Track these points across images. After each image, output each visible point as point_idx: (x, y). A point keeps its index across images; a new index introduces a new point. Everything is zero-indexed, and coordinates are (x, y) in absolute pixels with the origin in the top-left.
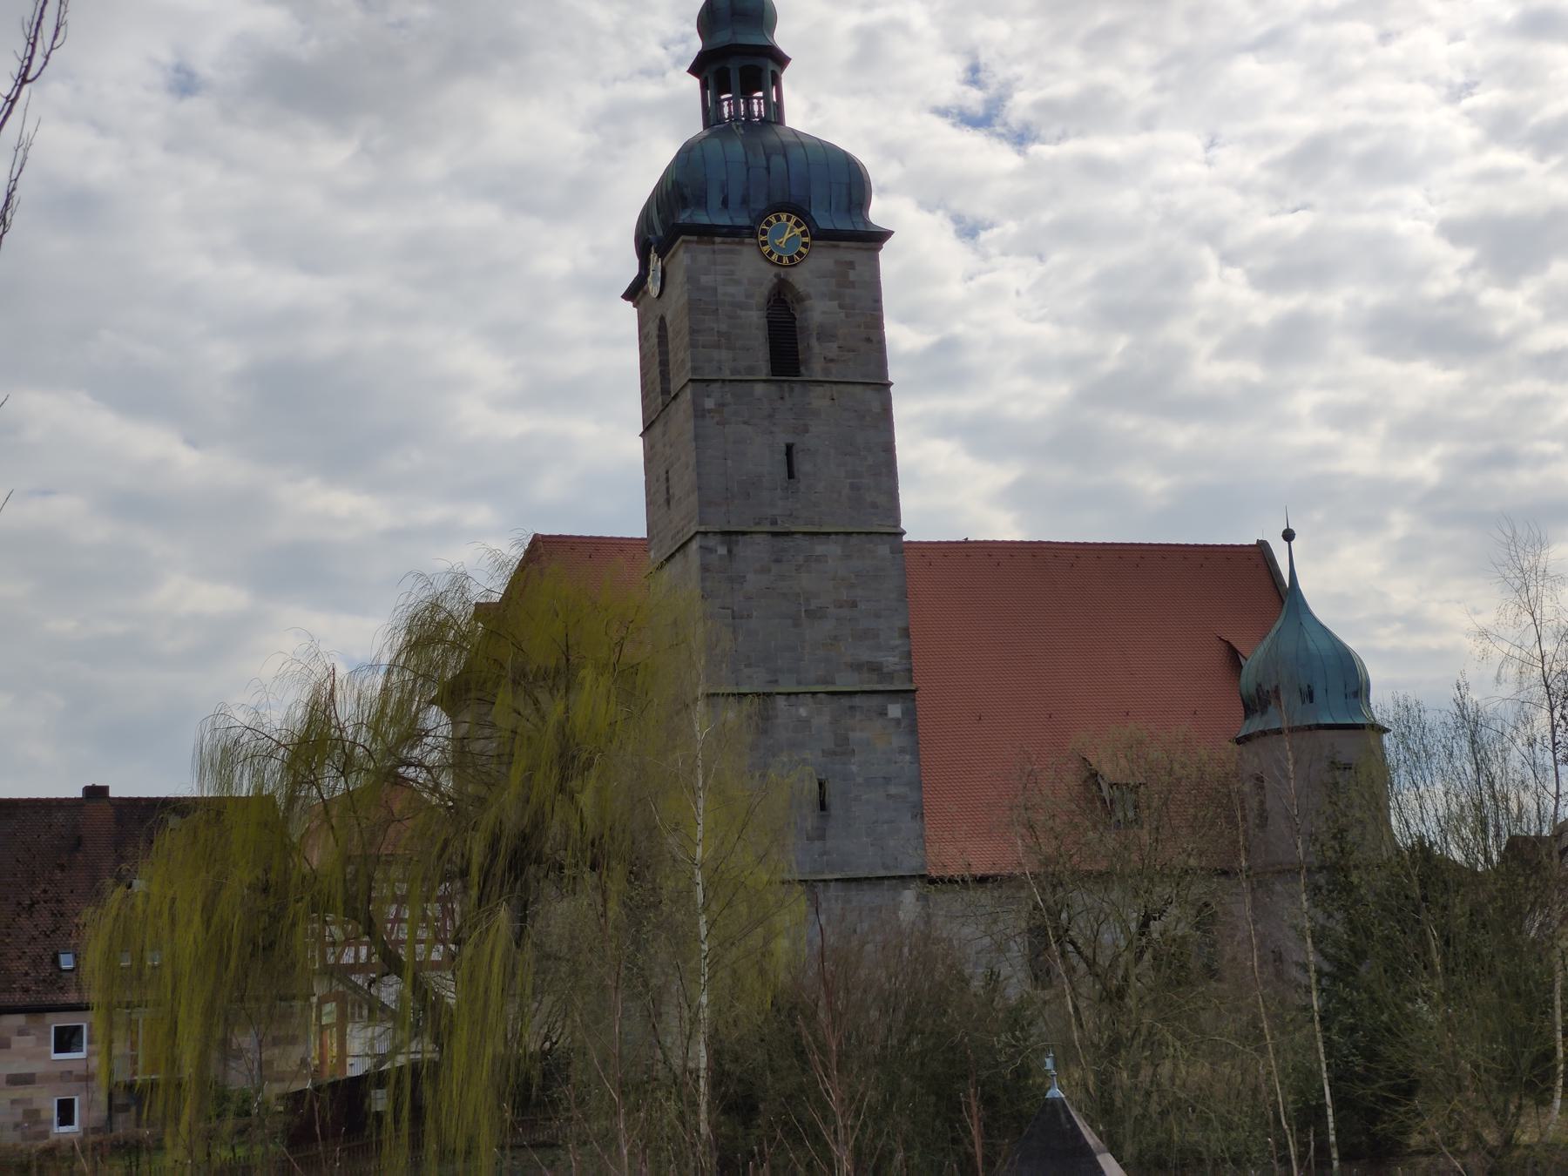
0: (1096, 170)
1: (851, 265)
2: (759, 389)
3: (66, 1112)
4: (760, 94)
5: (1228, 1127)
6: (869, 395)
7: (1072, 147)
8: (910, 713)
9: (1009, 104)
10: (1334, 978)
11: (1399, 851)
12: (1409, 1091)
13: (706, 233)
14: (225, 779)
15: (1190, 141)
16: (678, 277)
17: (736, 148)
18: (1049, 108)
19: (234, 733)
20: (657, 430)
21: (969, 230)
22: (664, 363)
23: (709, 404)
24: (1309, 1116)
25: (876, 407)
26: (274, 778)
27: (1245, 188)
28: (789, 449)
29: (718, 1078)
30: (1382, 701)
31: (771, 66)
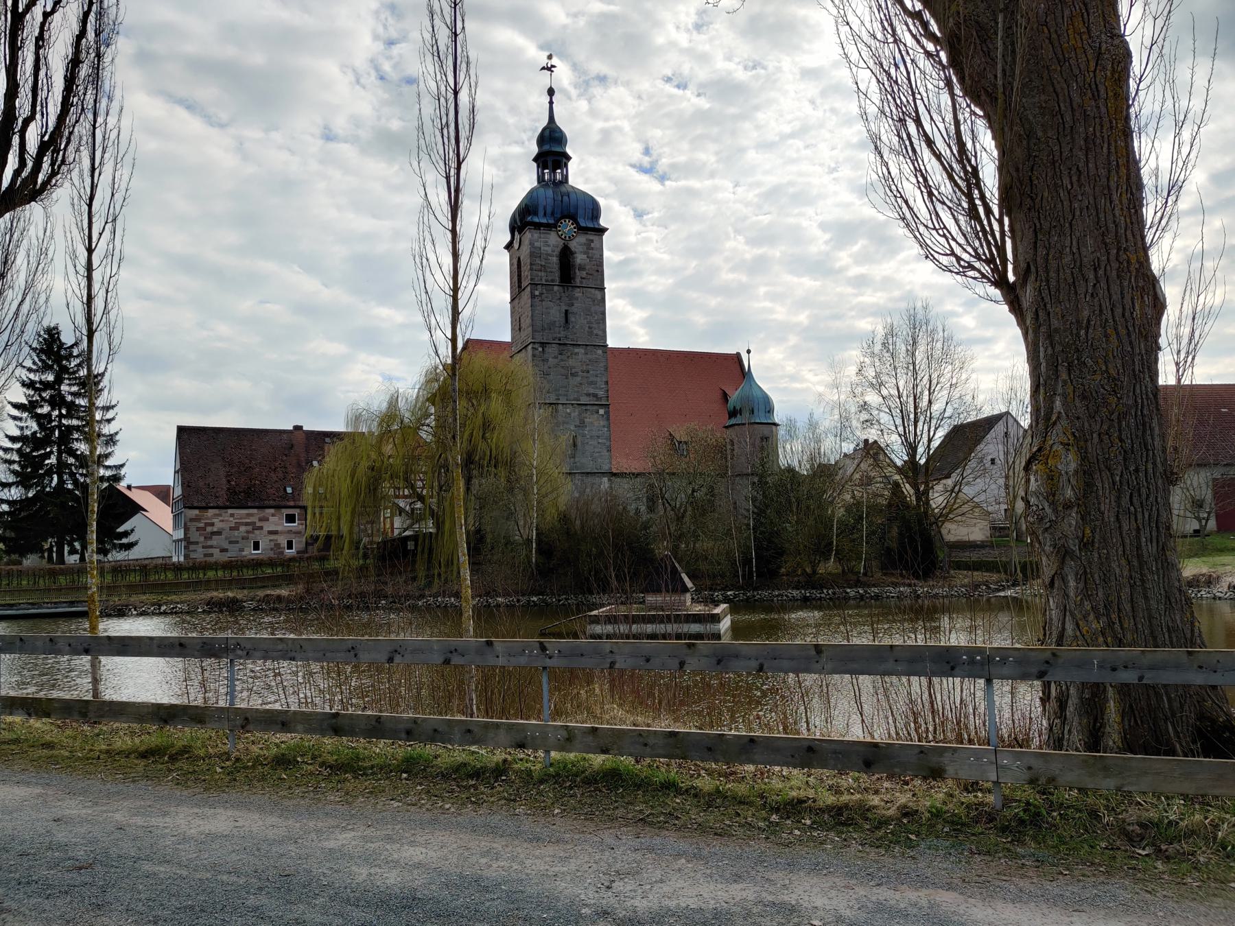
0: (691, 193)
1: (592, 241)
2: (556, 288)
3: (290, 545)
4: (559, 171)
5: (719, 564)
6: (597, 292)
7: (682, 183)
8: (607, 413)
9: (660, 163)
10: (758, 515)
11: (780, 467)
12: (781, 555)
13: (538, 226)
14: (356, 426)
15: (729, 185)
16: (526, 242)
17: (550, 193)
18: (674, 166)
19: (360, 411)
20: (516, 301)
21: (639, 215)
22: (519, 276)
23: (537, 293)
24: (747, 561)
25: (599, 297)
26: (375, 428)
27: (747, 204)
28: (566, 311)
29: (539, 542)
30: (779, 416)
31: (564, 160)
